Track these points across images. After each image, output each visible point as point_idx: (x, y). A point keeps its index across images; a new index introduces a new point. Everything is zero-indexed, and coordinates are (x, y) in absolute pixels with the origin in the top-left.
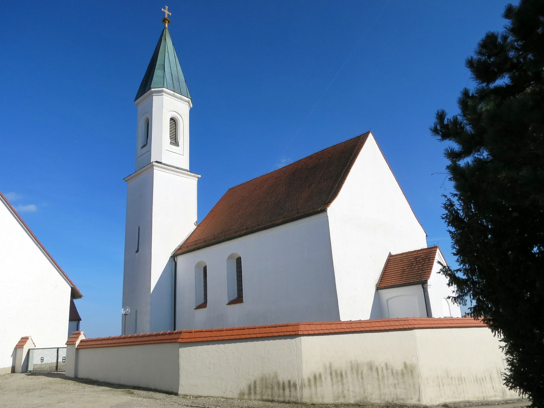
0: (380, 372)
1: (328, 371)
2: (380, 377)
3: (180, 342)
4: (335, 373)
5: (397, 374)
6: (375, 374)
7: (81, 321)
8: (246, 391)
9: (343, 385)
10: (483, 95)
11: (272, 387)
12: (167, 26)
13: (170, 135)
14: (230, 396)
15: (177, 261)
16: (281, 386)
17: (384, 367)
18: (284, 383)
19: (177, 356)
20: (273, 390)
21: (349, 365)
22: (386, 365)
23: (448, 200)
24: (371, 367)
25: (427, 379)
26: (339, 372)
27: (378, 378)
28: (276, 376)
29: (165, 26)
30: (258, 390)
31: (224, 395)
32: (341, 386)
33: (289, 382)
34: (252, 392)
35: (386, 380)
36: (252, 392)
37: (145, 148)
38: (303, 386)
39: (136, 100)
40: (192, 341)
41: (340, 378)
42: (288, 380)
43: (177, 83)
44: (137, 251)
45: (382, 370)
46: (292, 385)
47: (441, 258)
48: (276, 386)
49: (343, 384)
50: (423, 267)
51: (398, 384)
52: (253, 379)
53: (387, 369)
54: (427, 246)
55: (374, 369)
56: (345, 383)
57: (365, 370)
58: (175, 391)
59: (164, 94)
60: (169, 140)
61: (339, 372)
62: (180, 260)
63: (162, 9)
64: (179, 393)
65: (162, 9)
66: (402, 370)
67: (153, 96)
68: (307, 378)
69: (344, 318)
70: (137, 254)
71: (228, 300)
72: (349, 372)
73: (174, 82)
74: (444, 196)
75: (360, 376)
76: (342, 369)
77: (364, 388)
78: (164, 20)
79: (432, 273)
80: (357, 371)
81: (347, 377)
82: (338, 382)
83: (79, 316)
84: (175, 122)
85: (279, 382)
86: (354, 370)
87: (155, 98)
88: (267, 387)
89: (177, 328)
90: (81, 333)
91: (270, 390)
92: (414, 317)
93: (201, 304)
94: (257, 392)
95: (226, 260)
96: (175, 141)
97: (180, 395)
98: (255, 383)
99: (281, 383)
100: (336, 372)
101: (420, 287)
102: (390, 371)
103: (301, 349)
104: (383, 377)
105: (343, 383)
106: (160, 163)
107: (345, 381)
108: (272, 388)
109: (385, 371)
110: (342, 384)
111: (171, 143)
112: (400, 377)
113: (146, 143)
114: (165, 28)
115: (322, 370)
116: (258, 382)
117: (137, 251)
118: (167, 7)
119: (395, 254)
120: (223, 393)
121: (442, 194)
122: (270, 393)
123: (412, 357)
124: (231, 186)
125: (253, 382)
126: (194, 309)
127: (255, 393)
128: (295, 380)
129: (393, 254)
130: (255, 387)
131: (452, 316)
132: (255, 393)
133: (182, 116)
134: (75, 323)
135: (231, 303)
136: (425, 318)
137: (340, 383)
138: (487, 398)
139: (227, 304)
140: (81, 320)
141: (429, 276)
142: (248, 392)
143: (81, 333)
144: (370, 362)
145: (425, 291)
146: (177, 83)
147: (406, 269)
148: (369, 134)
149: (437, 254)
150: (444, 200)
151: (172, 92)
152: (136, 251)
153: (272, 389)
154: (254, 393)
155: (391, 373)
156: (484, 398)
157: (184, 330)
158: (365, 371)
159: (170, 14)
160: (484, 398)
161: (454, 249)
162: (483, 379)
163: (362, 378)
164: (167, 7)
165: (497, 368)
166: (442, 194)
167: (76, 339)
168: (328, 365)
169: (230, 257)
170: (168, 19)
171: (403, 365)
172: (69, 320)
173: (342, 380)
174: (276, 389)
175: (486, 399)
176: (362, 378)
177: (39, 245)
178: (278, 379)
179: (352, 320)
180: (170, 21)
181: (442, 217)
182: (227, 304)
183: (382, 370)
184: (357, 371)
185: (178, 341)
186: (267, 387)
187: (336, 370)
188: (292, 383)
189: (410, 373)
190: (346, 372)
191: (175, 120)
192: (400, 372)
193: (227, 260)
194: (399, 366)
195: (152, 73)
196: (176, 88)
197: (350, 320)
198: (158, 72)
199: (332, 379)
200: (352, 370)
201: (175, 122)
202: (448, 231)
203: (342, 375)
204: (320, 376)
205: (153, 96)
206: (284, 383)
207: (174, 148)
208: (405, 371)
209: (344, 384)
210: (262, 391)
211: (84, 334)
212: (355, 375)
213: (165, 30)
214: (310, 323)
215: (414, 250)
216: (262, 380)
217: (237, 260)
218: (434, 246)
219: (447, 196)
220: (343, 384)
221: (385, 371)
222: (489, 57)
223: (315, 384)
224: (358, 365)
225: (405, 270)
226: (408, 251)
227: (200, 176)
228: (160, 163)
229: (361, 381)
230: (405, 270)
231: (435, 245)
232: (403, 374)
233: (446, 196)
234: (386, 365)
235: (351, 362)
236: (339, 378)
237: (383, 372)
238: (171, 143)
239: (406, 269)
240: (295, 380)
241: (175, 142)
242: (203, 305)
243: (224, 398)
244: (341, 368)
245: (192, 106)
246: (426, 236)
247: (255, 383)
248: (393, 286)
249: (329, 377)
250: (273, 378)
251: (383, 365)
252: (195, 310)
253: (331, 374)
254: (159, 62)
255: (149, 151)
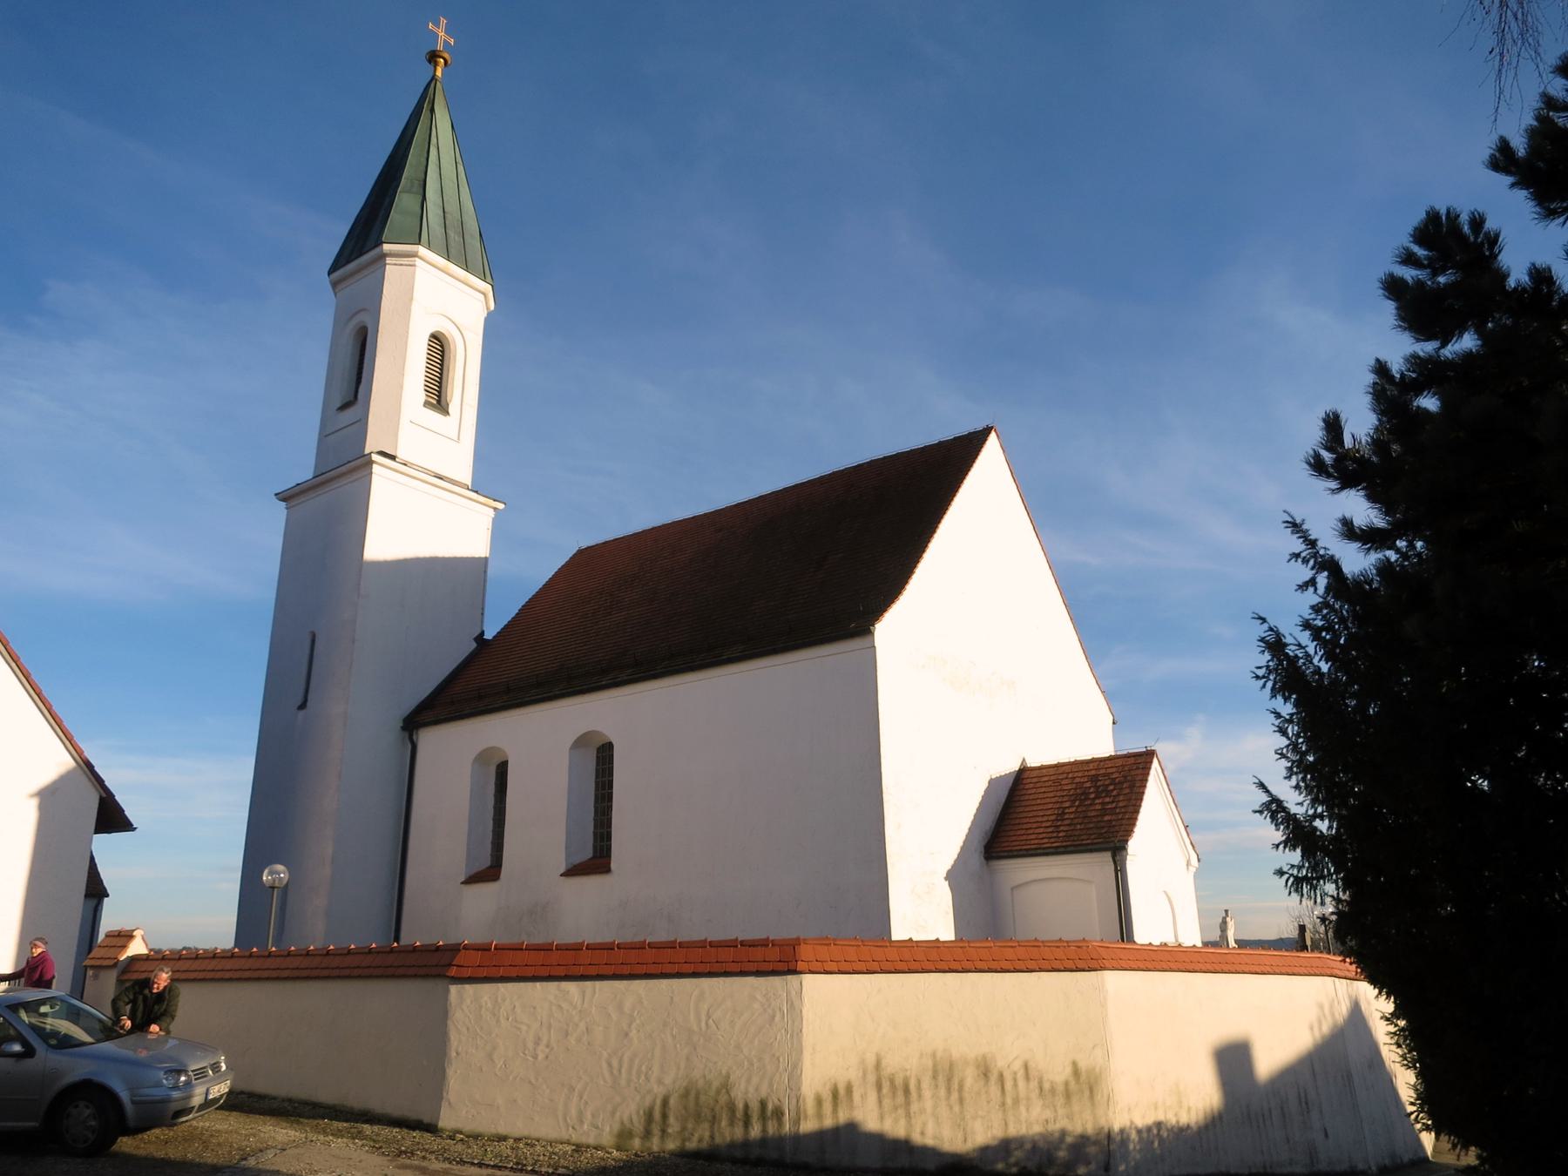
0: (1009, 1085)
1: (872, 1078)
2: (1009, 1101)
3: (453, 977)
4: (888, 1083)
5: (1053, 1091)
6: (994, 1089)
7: (106, 899)
8: (638, 1127)
9: (910, 1118)
10: (1427, 373)
11: (714, 1117)
12: (439, 73)
13: (426, 381)
14: (591, 1141)
15: (417, 739)
16: (740, 1114)
17: (1021, 1074)
18: (746, 1106)
19: (794, 1009)
20: (716, 1125)
21: (930, 1063)
22: (1026, 1067)
23: (1271, 629)
24: (985, 1070)
25: (1129, 1109)
26: (899, 1081)
27: (1003, 1104)
28: (726, 1086)
29: (435, 75)
30: (674, 1126)
31: (573, 1136)
32: (903, 1122)
33: (763, 1104)
34: (656, 1130)
35: (1023, 1109)
36: (656, 1130)
37: (350, 414)
38: (802, 1118)
39: (332, 273)
40: (243, 977)
41: (903, 1100)
42: (759, 1099)
43: (456, 238)
44: (303, 706)
45: (1015, 1080)
46: (769, 1113)
47: (1161, 784)
48: (724, 1116)
49: (908, 1115)
50: (1114, 805)
51: (1055, 1121)
52: (659, 1091)
53: (1027, 1078)
54: (1113, 750)
55: (994, 1078)
56: (915, 1113)
57: (970, 1077)
58: (426, 1120)
59: (417, 259)
60: (422, 396)
61: (899, 1081)
62: (432, 740)
63: (430, 24)
64: (441, 1124)
65: (430, 24)
66: (1067, 1084)
67: (385, 265)
68: (812, 1096)
69: (900, 930)
70: (301, 713)
71: (566, 860)
72: (926, 1084)
73: (451, 233)
74: (1260, 618)
75: (955, 1096)
76: (908, 1073)
77: (964, 1129)
78: (433, 57)
79: (1138, 823)
80: (949, 1080)
81: (920, 1096)
82: (896, 1108)
83: (102, 883)
84: (442, 346)
85: (734, 1104)
86: (940, 1078)
87: (392, 271)
88: (698, 1117)
89: (403, 934)
90: (135, 933)
91: (706, 1125)
92: (1084, 939)
93: (480, 869)
94: (670, 1131)
95: (568, 749)
96: (438, 400)
97: (442, 1130)
98: (665, 1102)
99: (740, 1106)
100: (892, 1081)
101: (1107, 856)
102: (1034, 1084)
103: (801, 1011)
104: (1016, 1101)
105: (909, 1113)
106: (393, 458)
107: (914, 1107)
108: (714, 1120)
109: (1021, 1084)
110: (906, 1116)
111: (427, 404)
112: (1060, 1100)
113: (352, 399)
114: (434, 78)
115: (853, 1075)
116: (672, 1102)
117: (303, 706)
118: (443, 21)
119: (1039, 765)
120: (571, 1129)
121: (1254, 613)
122: (707, 1134)
123: (1093, 1048)
124: (585, 544)
125: (658, 1102)
126: (462, 883)
127: (663, 1131)
128: (779, 1100)
129: (1033, 765)
130: (665, 1116)
131: (1181, 940)
132: (663, 1131)
133: (463, 332)
134: (93, 902)
135: (573, 871)
136: (1114, 943)
137: (901, 1112)
138: (1271, 1167)
139: (561, 875)
140: (108, 896)
141: (1132, 831)
142: (641, 1128)
143: (135, 933)
144: (984, 1057)
145: (1120, 870)
146: (456, 238)
147: (1068, 807)
148: (990, 433)
149: (1152, 772)
150: (1261, 630)
151: (442, 261)
152: (299, 704)
153: (714, 1124)
154: (660, 1133)
155: (1037, 1091)
156: (1265, 1167)
157: (466, 942)
158: (969, 1082)
159: (452, 42)
160: (1265, 1167)
161: (1283, 760)
162: (1263, 1116)
163: (961, 1100)
164: (443, 21)
165: (1298, 1088)
166: (1254, 613)
167: (120, 949)
168: (871, 1060)
169: (581, 742)
170: (446, 56)
171: (1069, 1070)
172: (86, 896)
173: (908, 1103)
174: (724, 1123)
175: (1269, 1170)
176: (961, 1100)
177: (13, 665)
178: (732, 1095)
179: (941, 939)
180: (449, 62)
181: (1254, 673)
182: (561, 875)
183: (1015, 1080)
184: (949, 1080)
185: (448, 974)
186: (698, 1117)
187: (893, 1074)
188: (770, 1107)
189: (1087, 1093)
190: (919, 1082)
191: (441, 339)
192: (1061, 1088)
193: (571, 749)
194: (1058, 1073)
195: (387, 200)
196: (452, 251)
197: (908, 938)
198: (404, 201)
199: (880, 1102)
200: (935, 1077)
201: (442, 346)
202: (1272, 712)
203: (907, 1091)
204: (849, 1089)
205: (387, 267)
206: (746, 1106)
207: (433, 416)
208: (1073, 1085)
209: (912, 1114)
210: (684, 1129)
211: (143, 939)
212: (942, 1092)
213: (432, 85)
214: (828, 942)
215: (1090, 758)
216: (685, 1094)
217: (598, 749)
218: (1144, 750)
219: (1268, 620)
220: (908, 1115)
221: (1021, 1084)
222: (1435, 273)
223: (833, 1113)
224: (951, 1066)
225: (1067, 811)
226: (1072, 760)
227: (501, 506)
228: (393, 458)
229: (957, 1108)
230: (1067, 811)
231: (1149, 749)
232: (1068, 1095)
233: (1264, 620)
234: (1026, 1067)
235: (934, 1055)
236: (900, 1099)
237: (1015, 1085)
238: (427, 404)
239: (1068, 807)
240: (779, 1100)
241: (435, 402)
242: (490, 873)
243: (573, 1145)
244: (906, 1070)
245: (492, 306)
246: (1114, 723)
247: (665, 1102)
248: (1033, 852)
249: (872, 1097)
250: (718, 1092)
251: (1017, 1065)
252: (463, 885)
253: (879, 1087)
254: (408, 173)
255: (362, 422)
